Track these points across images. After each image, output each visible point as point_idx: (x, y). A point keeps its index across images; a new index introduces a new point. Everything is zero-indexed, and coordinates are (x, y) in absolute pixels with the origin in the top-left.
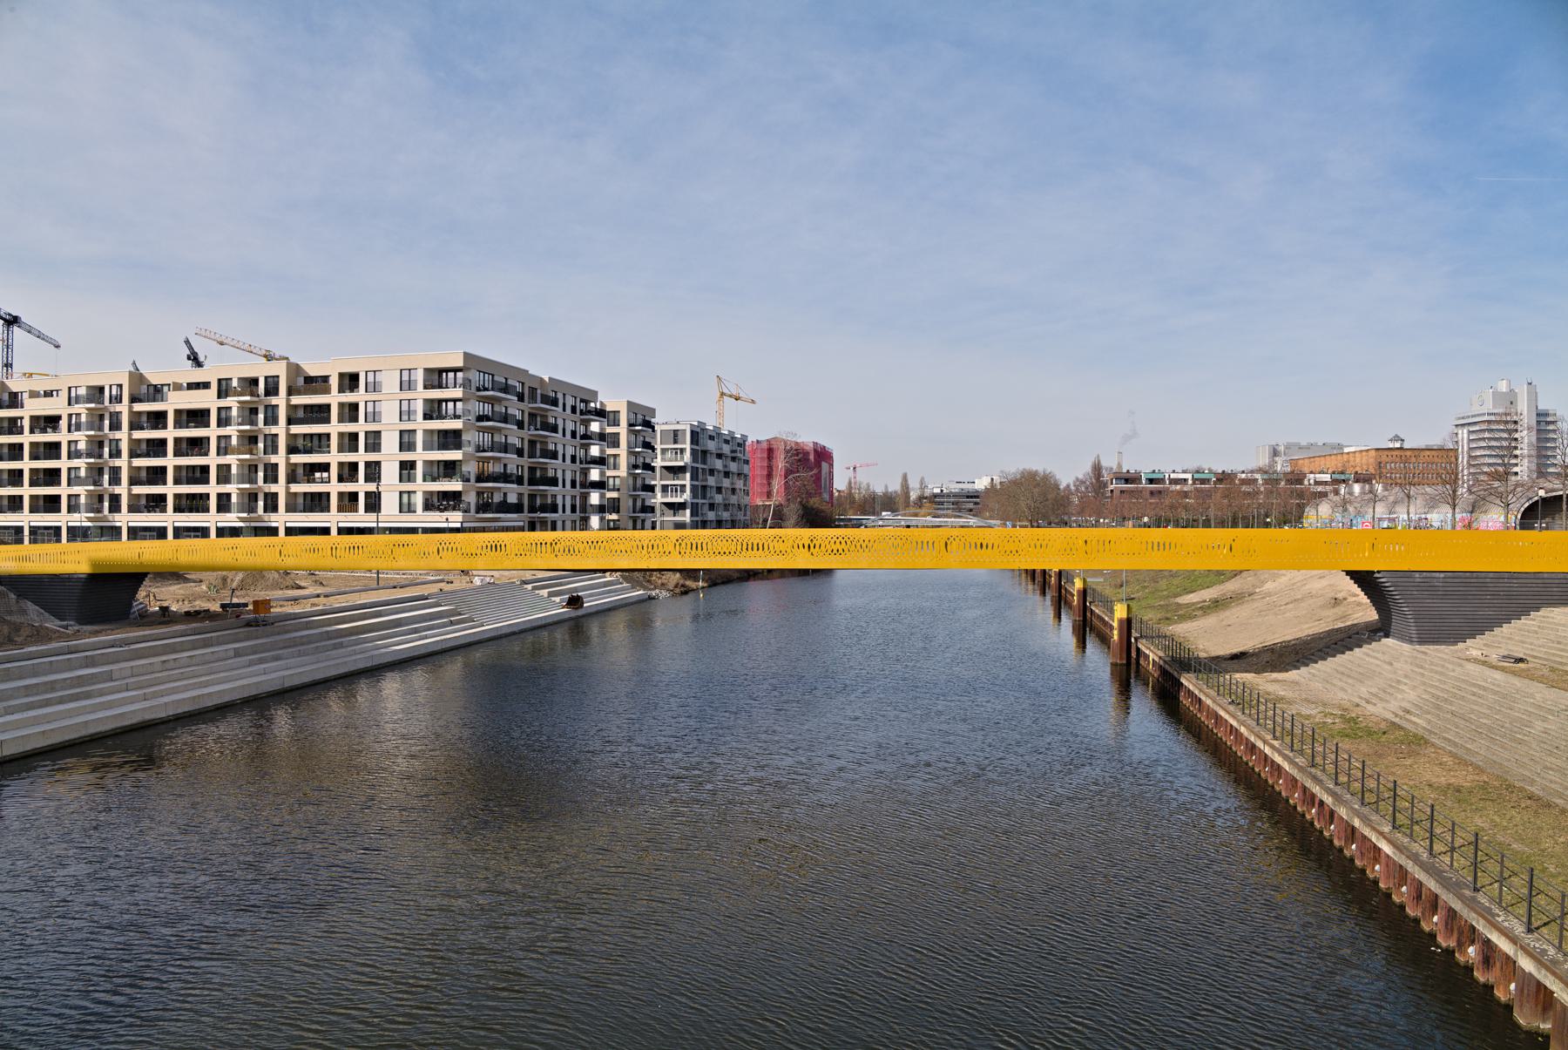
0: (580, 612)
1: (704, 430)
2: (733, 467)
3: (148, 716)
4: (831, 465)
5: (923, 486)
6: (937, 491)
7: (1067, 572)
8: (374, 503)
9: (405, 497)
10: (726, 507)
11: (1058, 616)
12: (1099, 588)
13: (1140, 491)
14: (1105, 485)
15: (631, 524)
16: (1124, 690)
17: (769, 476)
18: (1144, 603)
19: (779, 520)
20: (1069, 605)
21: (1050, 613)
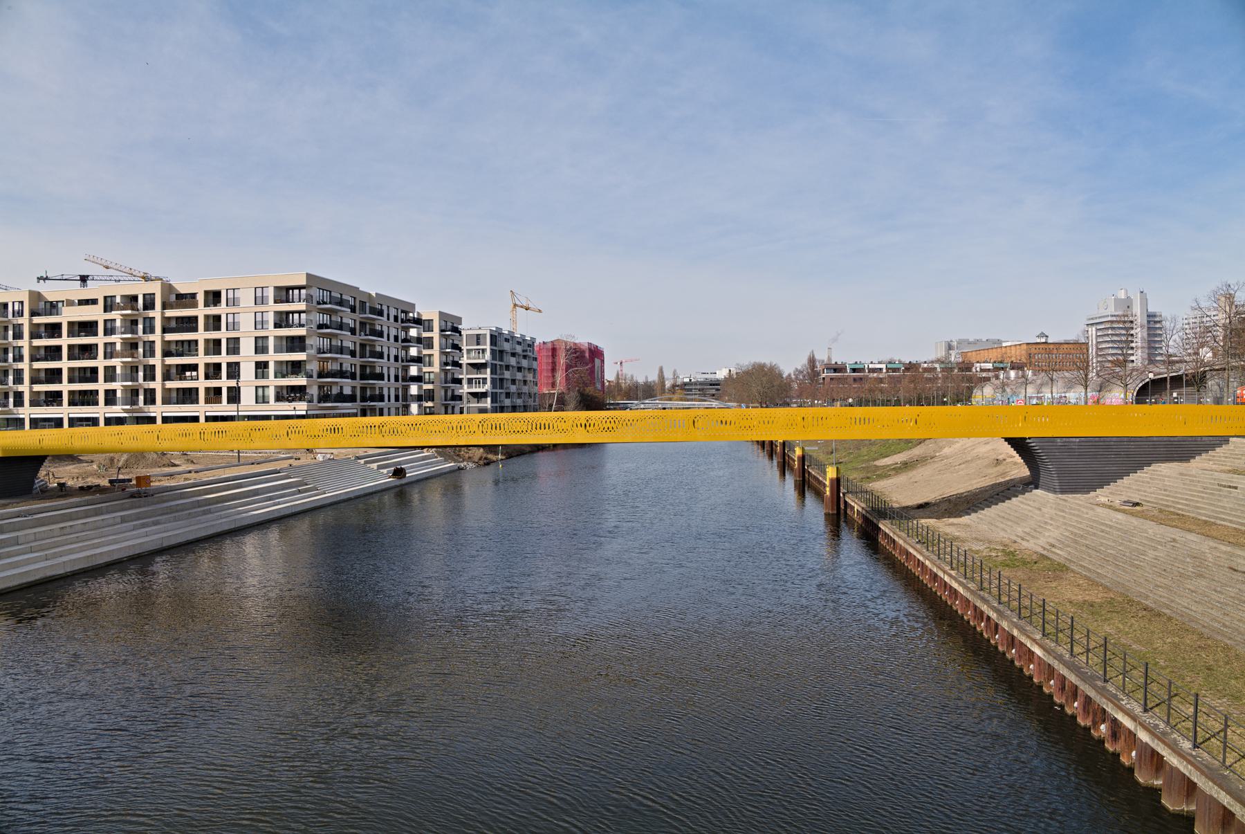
0: (403, 481)
1: (501, 334)
2: (525, 363)
3: (49, 573)
4: (603, 361)
5: (675, 377)
6: (687, 380)
7: (790, 443)
8: (234, 396)
9: (260, 391)
10: (519, 395)
11: (783, 474)
12: (814, 455)
13: (846, 378)
14: (818, 374)
15: (443, 410)
16: (836, 534)
17: (554, 370)
18: (850, 466)
19: (562, 405)
20: (792, 469)
21: (777, 473)
